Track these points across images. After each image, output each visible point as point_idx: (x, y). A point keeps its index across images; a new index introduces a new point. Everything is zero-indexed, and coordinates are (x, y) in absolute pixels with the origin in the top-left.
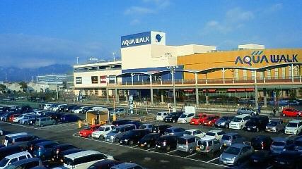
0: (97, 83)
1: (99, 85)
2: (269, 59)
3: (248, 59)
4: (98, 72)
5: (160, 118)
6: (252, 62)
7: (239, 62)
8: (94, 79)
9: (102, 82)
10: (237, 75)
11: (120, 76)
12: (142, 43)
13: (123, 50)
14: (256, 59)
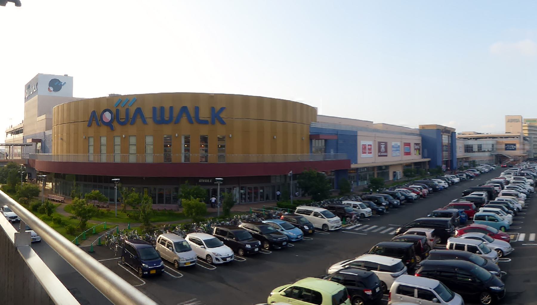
2: (148, 113)
7: (94, 123)
14: (122, 115)
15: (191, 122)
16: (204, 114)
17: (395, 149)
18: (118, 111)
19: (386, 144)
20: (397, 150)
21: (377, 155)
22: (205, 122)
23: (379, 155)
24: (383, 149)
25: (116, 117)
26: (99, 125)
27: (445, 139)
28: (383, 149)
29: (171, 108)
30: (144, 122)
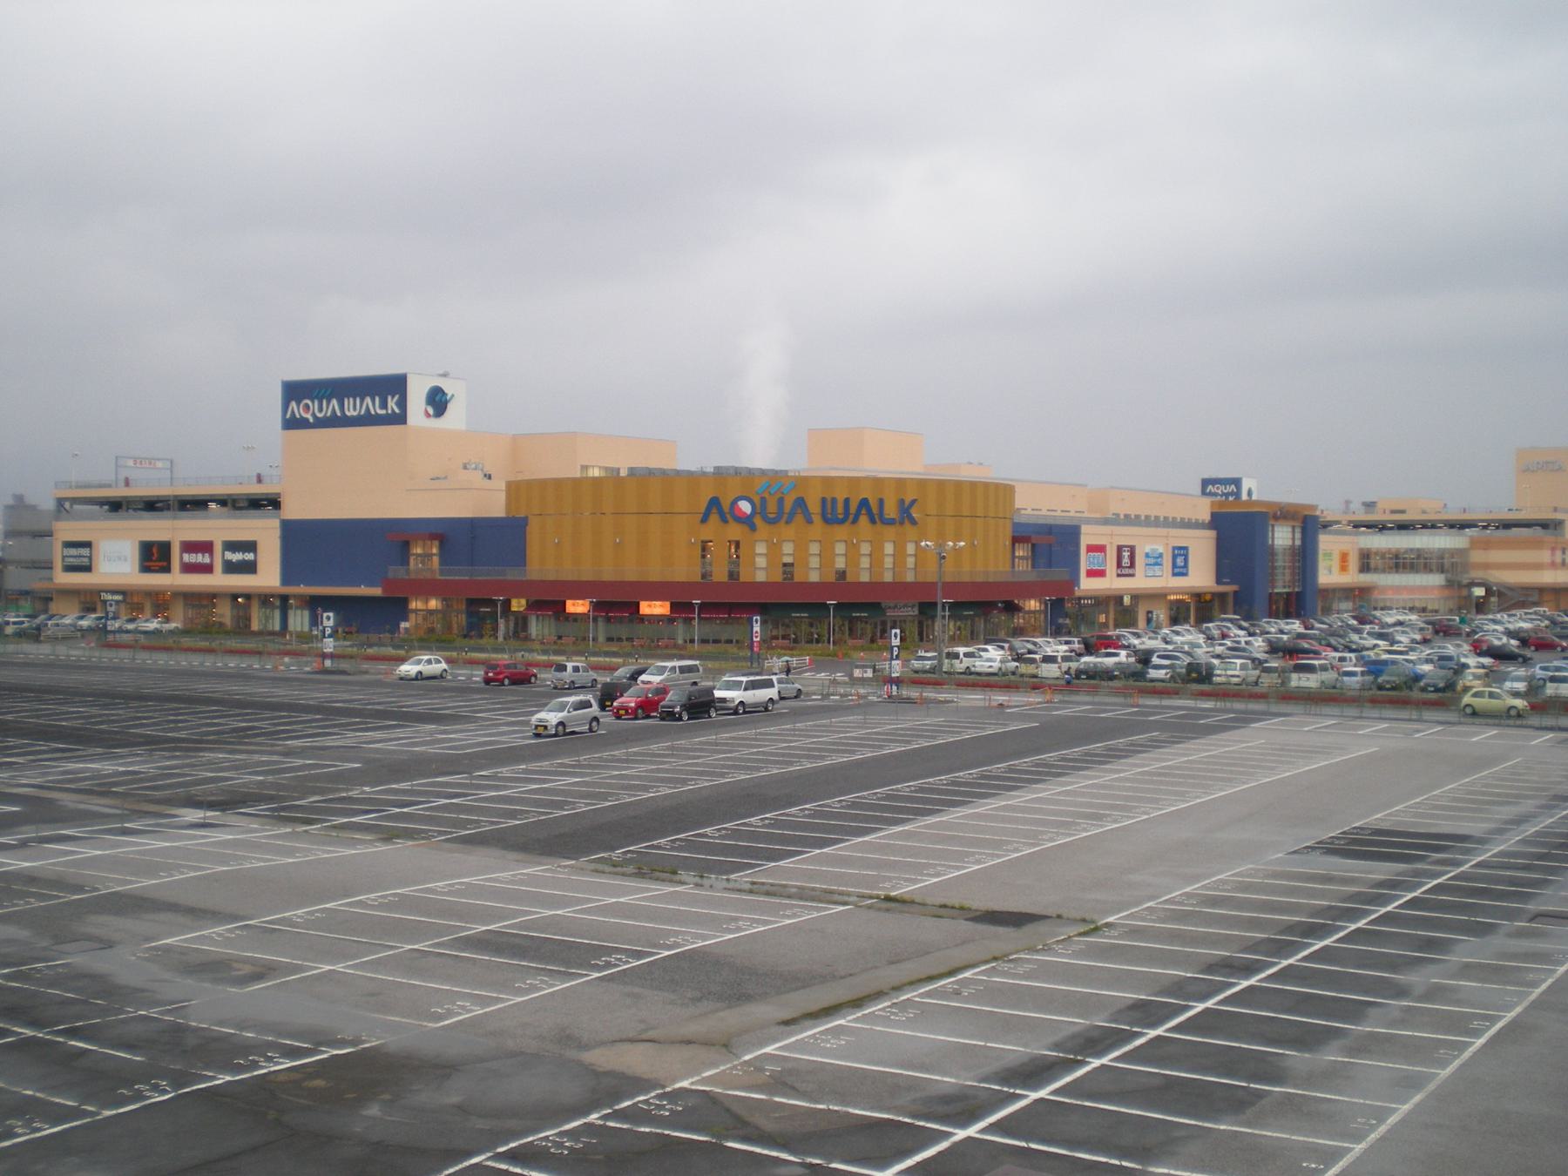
1: (176, 579)
2: (814, 507)
6: (758, 521)
7: (714, 518)
8: (155, 556)
9: (189, 568)
11: (1343, 645)
12: (368, 420)
14: (772, 507)
15: (873, 521)
16: (891, 511)
17: (1152, 561)
18: (763, 500)
19: (1132, 550)
20: (1156, 564)
21: (1115, 575)
22: (891, 522)
23: (1119, 572)
24: (1126, 561)
25: (760, 508)
26: (725, 521)
27: (1283, 537)
28: (1126, 561)
30: (810, 521)
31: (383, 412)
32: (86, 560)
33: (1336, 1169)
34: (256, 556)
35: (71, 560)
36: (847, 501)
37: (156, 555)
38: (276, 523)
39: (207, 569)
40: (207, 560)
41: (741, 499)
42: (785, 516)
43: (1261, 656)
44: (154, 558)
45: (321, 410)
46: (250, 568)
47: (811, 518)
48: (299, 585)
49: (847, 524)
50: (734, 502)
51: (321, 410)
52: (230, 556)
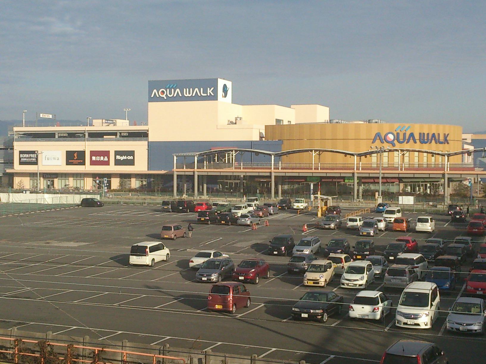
0: (83, 164)
2: (417, 137)
3: (391, 137)
4: (87, 143)
5: (198, 261)
10: (385, 160)
12: (197, 98)
13: (153, 106)
14: (401, 137)
15: (436, 143)
16: (442, 138)
22: (441, 143)
29: (428, 134)
30: (415, 142)
31: (205, 95)
32: (35, 159)
33: (324, 362)
34: (134, 158)
35: (25, 159)
36: (428, 134)
37: (76, 157)
38: (146, 143)
39: (107, 163)
40: (106, 159)
41: (389, 134)
42: (406, 140)
43: (468, 192)
44: (75, 159)
45: (170, 93)
46: (131, 163)
47: (416, 141)
48: (162, 170)
49: (428, 143)
50: (386, 135)
51: (170, 93)
52: (118, 157)
